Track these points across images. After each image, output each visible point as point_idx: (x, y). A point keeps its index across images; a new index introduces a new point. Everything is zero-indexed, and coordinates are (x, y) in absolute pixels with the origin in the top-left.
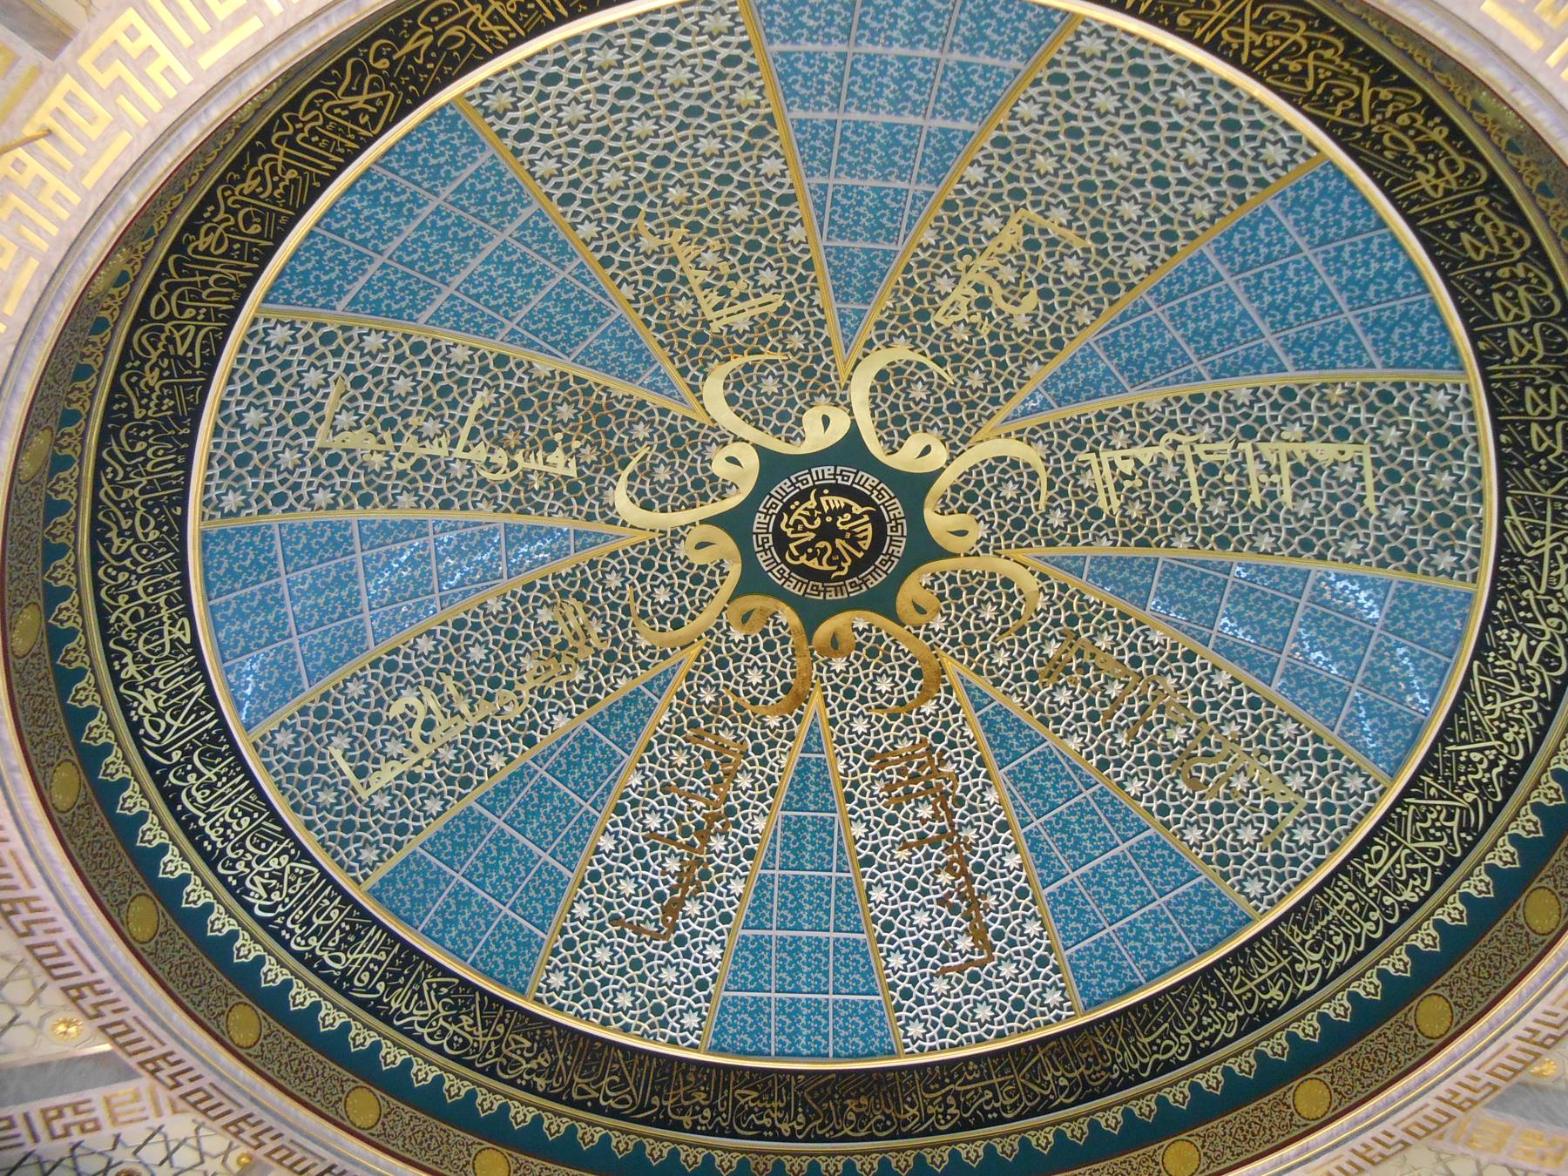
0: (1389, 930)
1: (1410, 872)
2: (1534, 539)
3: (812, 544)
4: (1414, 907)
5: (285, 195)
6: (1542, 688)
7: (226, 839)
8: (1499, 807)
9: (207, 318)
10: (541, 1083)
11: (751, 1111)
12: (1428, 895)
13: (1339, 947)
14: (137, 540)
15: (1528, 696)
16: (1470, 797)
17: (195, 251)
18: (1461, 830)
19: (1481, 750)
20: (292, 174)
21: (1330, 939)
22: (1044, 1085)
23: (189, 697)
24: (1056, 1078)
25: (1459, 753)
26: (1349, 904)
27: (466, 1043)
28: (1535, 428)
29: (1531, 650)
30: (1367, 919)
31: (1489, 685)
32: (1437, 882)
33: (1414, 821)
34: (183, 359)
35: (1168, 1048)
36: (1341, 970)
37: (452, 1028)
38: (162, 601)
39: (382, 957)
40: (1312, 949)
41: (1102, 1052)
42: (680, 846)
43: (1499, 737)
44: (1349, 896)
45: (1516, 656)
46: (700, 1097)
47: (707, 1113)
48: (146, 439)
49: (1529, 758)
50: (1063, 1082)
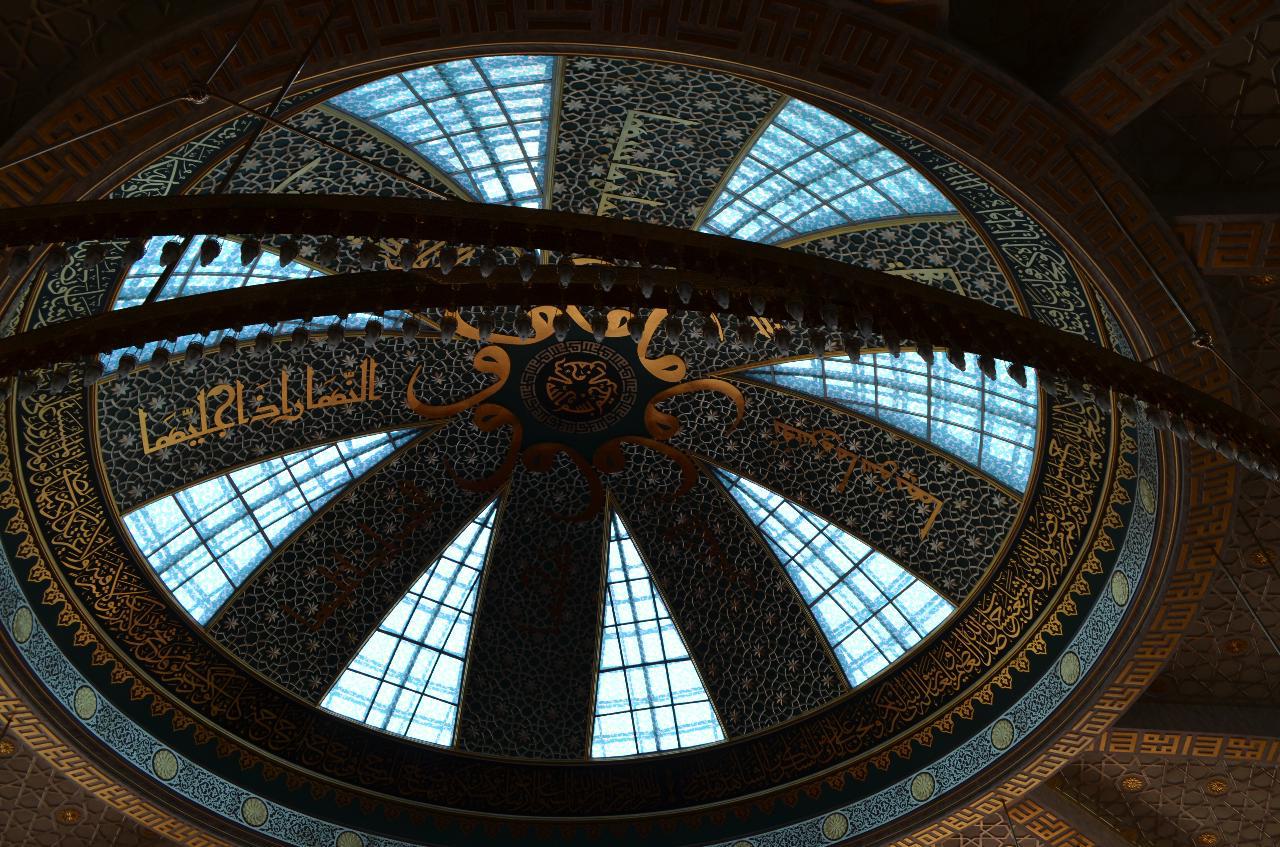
0: (27, 473)
1: (57, 503)
2: (217, 678)
3: (589, 377)
4: (33, 497)
5: (931, 666)
6: (132, 639)
8: (71, 581)
9: (983, 618)
12: (36, 510)
13: (37, 433)
14: (1060, 521)
15: (130, 628)
16: (86, 563)
17: (977, 661)
18: (68, 549)
19: (111, 584)
20: (926, 677)
21: (47, 428)
23: (1064, 409)
25: (116, 569)
26: (62, 451)
28: (274, 717)
29: (156, 643)
30: (44, 460)
31: (148, 607)
32: (41, 520)
33: (89, 520)
36: (22, 427)
38: (1060, 476)
40: (50, 411)
43: (114, 599)
44: (67, 453)
45: (157, 632)
48: (1033, 574)
49: (93, 612)
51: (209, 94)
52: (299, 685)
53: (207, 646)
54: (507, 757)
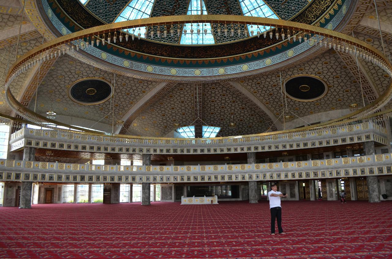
7: (155, 51)
10: (226, 54)
11: (262, 43)
22: (310, 18)
24: (311, 16)
27: (210, 55)
34: (85, 17)
35: (327, 3)
37: (207, 54)
39: (189, 50)
41: (317, 8)
42: (223, 7)
46: (253, 45)
47: (255, 47)
50: (312, 16)
51: (121, 42)
52: (173, 41)
53: (147, 42)
54: (295, 15)
